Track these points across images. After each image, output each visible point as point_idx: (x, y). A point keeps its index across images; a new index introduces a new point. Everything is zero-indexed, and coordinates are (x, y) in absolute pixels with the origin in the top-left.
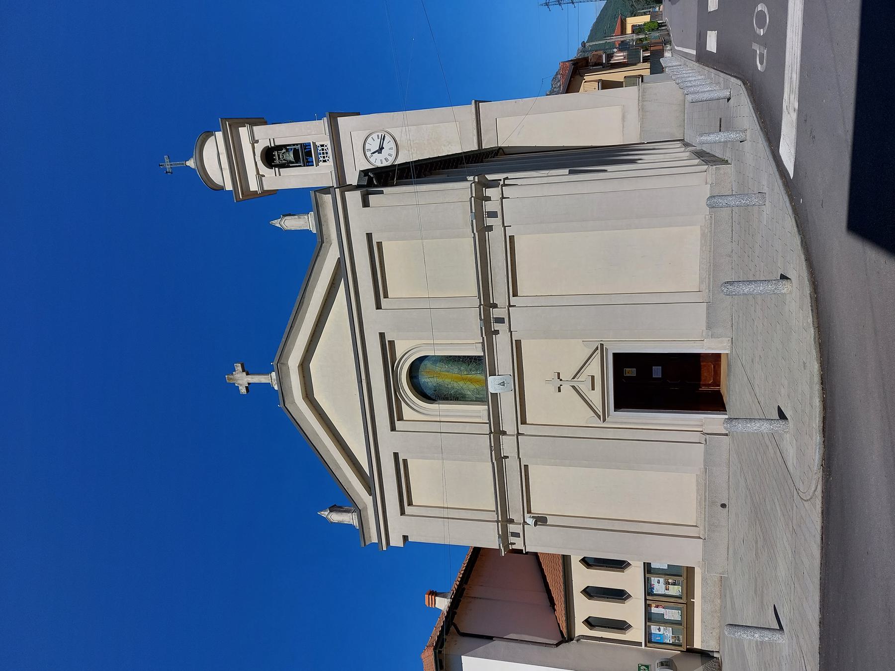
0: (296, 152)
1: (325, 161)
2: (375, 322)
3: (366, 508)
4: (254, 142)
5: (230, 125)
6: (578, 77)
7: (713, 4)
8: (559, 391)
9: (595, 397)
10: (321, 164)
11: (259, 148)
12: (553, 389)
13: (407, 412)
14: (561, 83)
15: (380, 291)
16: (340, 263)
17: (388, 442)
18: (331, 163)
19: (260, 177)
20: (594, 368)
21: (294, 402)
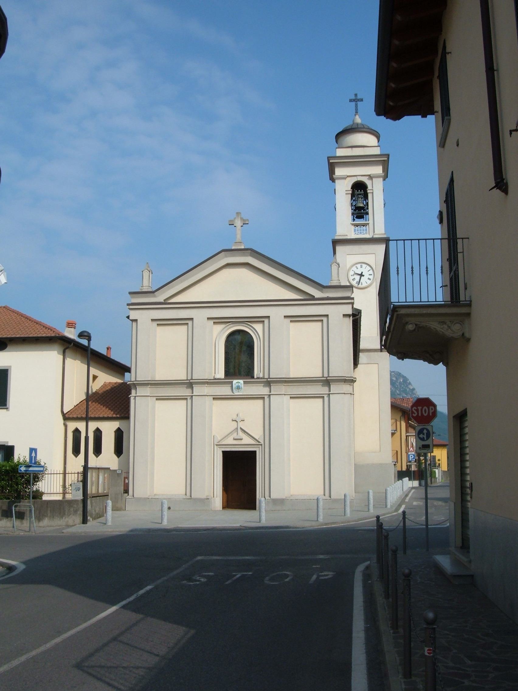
0: (362, 208)
1: (355, 231)
2: (276, 314)
3: (155, 296)
4: (370, 177)
5: (384, 160)
6: (400, 414)
7: (2, 504)
8: (233, 420)
9: (230, 441)
10: (353, 227)
11: (365, 180)
12: (235, 417)
13: (219, 327)
14: (399, 402)
15: (294, 319)
16: (313, 298)
17: (200, 316)
18: (353, 236)
19: (344, 178)
20: (247, 440)
21: (226, 257)
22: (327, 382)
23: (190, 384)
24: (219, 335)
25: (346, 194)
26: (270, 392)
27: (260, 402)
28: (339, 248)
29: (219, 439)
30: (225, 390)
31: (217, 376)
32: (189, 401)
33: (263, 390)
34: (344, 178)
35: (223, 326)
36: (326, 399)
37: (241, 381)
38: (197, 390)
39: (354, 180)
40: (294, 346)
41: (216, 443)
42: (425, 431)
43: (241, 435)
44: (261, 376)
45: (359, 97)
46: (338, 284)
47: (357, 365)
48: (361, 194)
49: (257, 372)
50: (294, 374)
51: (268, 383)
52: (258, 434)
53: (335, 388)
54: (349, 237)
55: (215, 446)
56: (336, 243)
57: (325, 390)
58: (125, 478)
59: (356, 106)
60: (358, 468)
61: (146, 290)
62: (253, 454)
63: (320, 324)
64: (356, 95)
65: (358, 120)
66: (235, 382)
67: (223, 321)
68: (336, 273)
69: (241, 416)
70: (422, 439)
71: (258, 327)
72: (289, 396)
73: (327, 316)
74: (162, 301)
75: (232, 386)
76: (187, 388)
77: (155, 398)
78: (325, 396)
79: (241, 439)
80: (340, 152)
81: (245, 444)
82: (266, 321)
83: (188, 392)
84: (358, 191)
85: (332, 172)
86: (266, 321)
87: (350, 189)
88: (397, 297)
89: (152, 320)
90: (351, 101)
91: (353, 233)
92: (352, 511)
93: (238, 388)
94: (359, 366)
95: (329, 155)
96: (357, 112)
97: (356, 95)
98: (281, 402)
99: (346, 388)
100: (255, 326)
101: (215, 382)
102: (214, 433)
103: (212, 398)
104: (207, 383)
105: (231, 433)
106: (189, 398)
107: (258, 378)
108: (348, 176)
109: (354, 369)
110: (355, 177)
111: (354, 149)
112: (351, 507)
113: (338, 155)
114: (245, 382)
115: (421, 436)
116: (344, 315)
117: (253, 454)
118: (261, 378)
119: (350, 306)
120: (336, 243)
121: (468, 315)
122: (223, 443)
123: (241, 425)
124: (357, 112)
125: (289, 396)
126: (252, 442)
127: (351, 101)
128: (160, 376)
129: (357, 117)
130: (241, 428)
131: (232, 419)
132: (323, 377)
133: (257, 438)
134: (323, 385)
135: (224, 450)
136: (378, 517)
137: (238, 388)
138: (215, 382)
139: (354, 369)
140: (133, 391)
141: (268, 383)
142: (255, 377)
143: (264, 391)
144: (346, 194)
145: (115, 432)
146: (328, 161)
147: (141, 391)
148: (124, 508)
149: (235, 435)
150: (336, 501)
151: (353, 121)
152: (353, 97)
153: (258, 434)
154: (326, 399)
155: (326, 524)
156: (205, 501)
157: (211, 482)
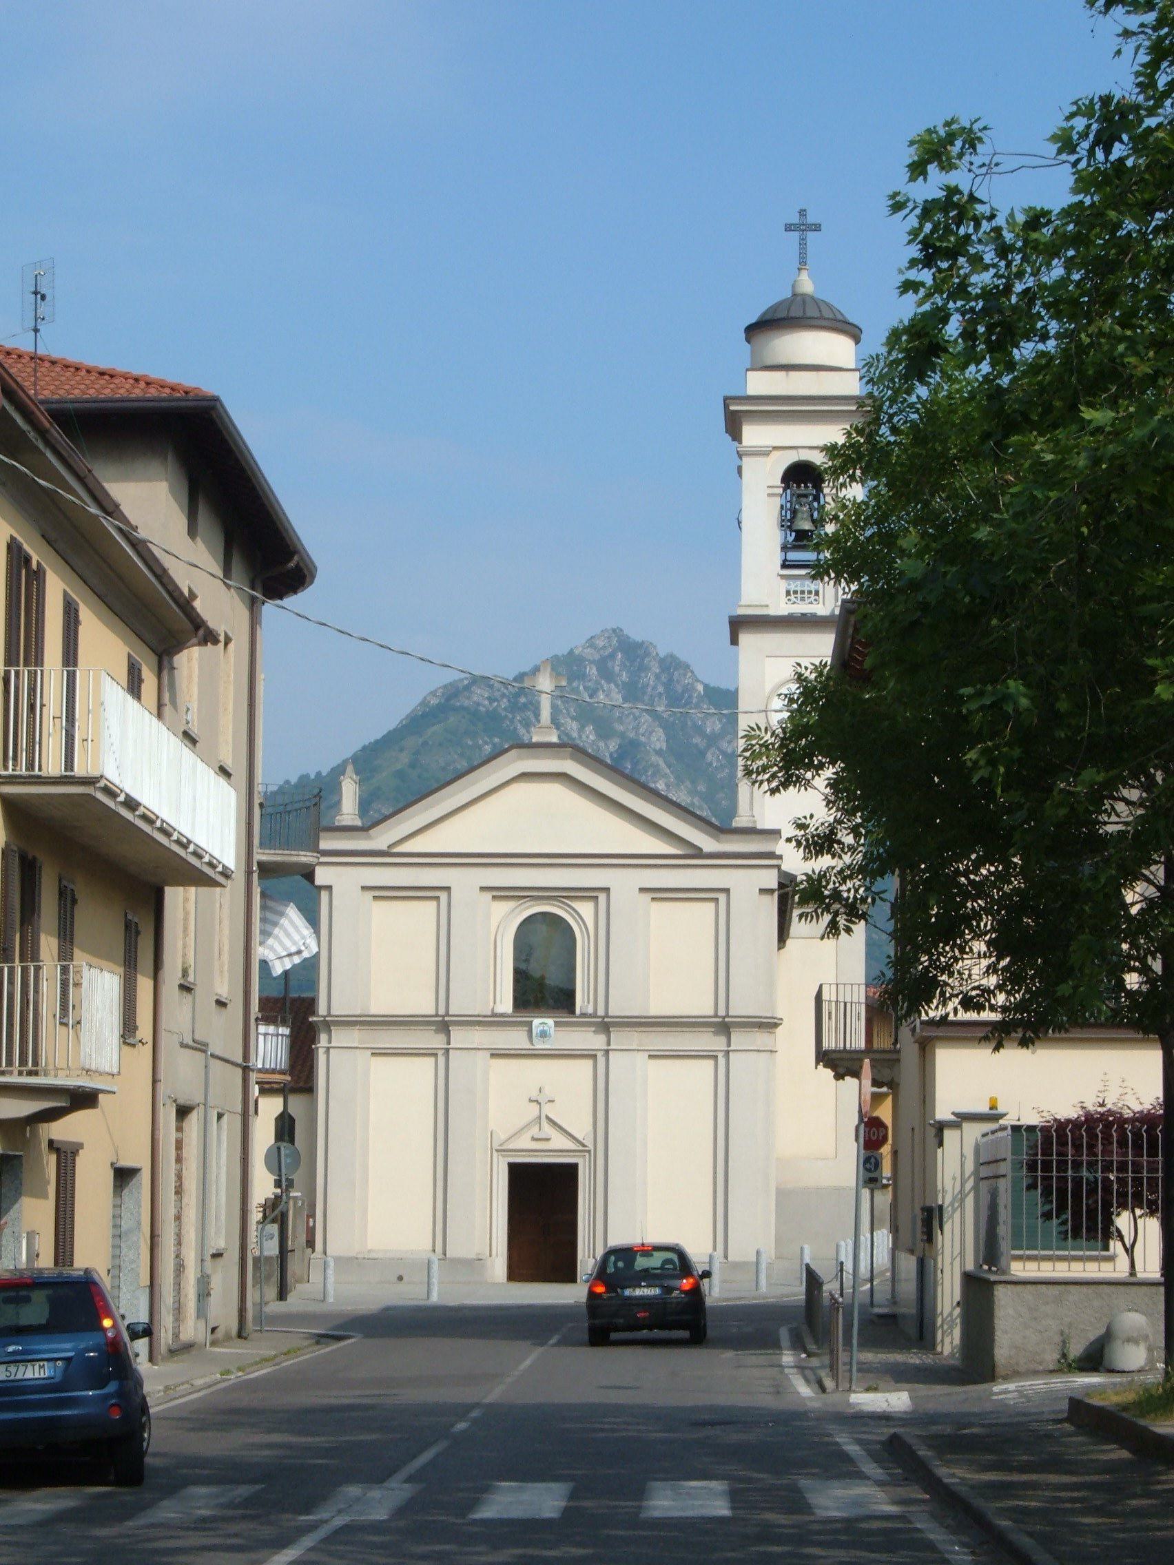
2: (623, 883)
3: (370, 838)
8: (531, 1101)
12: (534, 1095)
13: (504, 907)
15: (659, 894)
16: (698, 853)
17: (464, 882)
18: (782, 607)
19: (763, 453)
21: (520, 758)
22: (724, 1027)
23: (444, 1025)
24: (505, 921)
25: (769, 495)
26: (609, 1044)
27: (587, 1064)
28: (744, 638)
29: (503, 1137)
30: (515, 1039)
31: (500, 1009)
32: (441, 1059)
33: (592, 1040)
34: (763, 453)
35: (511, 904)
36: (721, 1061)
37: (550, 1022)
38: (459, 1037)
39: (791, 458)
40: (657, 952)
41: (495, 1146)
42: (873, 1160)
43: (548, 1130)
44: (590, 1010)
45: (811, 219)
46: (750, 825)
47: (784, 942)
48: (806, 496)
49: (581, 1002)
50: (657, 1008)
51: (605, 1026)
52: (581, 1127)
53: (739, 1039)
54: (772, 612)
55: (495, 1154)
56: (739, 625)
57: (719, 1043)
58: (308, 1217)
59: (803, 243)
60: (784, 1196)
61: (350, 823)
62: (570, 1172)
63: (712, 905)
64: (802, 213)
65: (807, 285)
66: (536, 1022)
67: (512, 894)
68: (748, 801)
69: (548, 1093)
70: (869, 1170)
71: (586, 909)
72: (646, 1054)
73: (727, 891)
74: (385, 848)
75: (530, 1032)
76: (437, 1031)
77: (369, 1052)
78: (720, 1055)
79: (548, 1140)
80: (760, 384)
81: (553, 1148)
82: (602, 897)
83: (437, 1041)
84: (798, 487)
85: (736, 434)
86: (602, 897)
87: (778, 482)
88: (825, 1045)
89: (364, 888)
90: (789, 228)
91: (782, 605)
92: (769, 1284)
93: (544, 1035)
94: (789, 942)
95: (729, 394)
96: (803, 262)
97: (802, 213)
98: (631, 1066)
99: (760, 1039)
100: (578, 905)
101: (493, 1021)
102: (492, 1125)
103: (487, 1054)
104: (479, 1023)
105: (527, 1126)
106: (440, 1053)
107: (584, 1015)
108: (775, 448)
109: (779, 949)
110: (794, 452)
111: (793, 374)
112: (768, 1277)
113: (751, 391)
114: (557, 1024)
115: (868, 1166)
116: (762, 891)
117: (570, 1172)
118: (590, 1016)
119: (775, 871)
120: (739, 625)
121: (898, 1060)
122: (511, 1147)
123: (548, 1110)
124: (803, 262)
125: (646, 1054)
126: (570, 1145)
127: (789, 228)
128: (379, 1006)
129: (804, 276)
130: (547, 1117)
131: (528, 1098)
132: (716, 1016)
133: (580, 1138)
134: (716, 1033)
135: (512, 1160)
136: (813, 1281)
137: (544, 1035)
138: (493, 1021)
139: (779, 949)
140: (323, 1038)
141: (605, 1026)
142: (578, 1011)
143: (595, 1041)
144: (769, 495)
145: (276, 1119)
146: (726, 406)
147: (340, 1037)
148: (306, 1277)
149: (534, 1131)
150: (737, 1266)
151: (793, 286)
152: (795, 219)
153: (581, 1127)
154: (721, 1061)
155: (727, 1300)
156: (475, 1264)
157: (485, 1227)
